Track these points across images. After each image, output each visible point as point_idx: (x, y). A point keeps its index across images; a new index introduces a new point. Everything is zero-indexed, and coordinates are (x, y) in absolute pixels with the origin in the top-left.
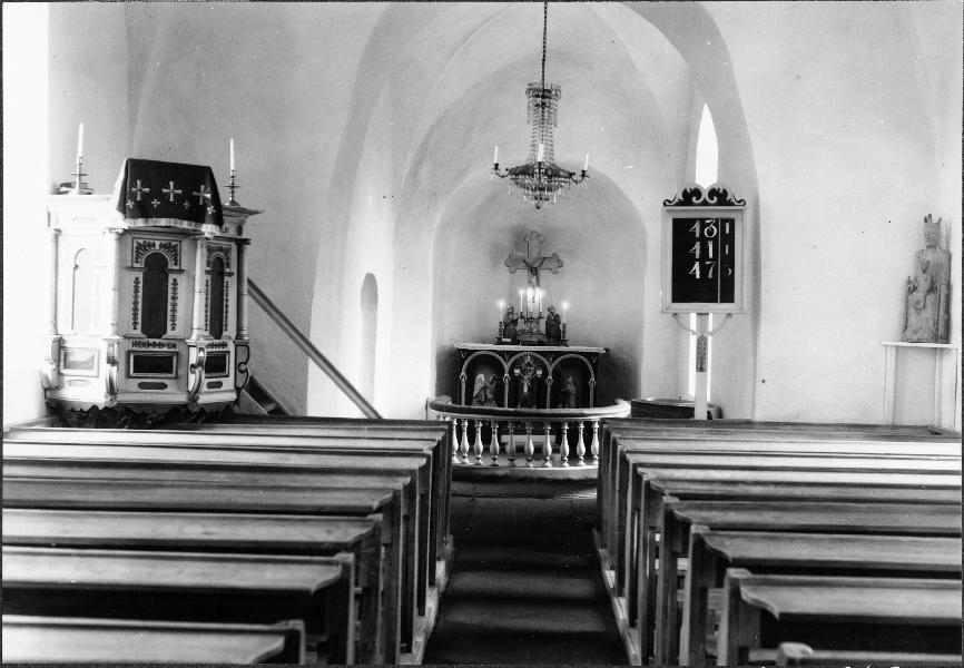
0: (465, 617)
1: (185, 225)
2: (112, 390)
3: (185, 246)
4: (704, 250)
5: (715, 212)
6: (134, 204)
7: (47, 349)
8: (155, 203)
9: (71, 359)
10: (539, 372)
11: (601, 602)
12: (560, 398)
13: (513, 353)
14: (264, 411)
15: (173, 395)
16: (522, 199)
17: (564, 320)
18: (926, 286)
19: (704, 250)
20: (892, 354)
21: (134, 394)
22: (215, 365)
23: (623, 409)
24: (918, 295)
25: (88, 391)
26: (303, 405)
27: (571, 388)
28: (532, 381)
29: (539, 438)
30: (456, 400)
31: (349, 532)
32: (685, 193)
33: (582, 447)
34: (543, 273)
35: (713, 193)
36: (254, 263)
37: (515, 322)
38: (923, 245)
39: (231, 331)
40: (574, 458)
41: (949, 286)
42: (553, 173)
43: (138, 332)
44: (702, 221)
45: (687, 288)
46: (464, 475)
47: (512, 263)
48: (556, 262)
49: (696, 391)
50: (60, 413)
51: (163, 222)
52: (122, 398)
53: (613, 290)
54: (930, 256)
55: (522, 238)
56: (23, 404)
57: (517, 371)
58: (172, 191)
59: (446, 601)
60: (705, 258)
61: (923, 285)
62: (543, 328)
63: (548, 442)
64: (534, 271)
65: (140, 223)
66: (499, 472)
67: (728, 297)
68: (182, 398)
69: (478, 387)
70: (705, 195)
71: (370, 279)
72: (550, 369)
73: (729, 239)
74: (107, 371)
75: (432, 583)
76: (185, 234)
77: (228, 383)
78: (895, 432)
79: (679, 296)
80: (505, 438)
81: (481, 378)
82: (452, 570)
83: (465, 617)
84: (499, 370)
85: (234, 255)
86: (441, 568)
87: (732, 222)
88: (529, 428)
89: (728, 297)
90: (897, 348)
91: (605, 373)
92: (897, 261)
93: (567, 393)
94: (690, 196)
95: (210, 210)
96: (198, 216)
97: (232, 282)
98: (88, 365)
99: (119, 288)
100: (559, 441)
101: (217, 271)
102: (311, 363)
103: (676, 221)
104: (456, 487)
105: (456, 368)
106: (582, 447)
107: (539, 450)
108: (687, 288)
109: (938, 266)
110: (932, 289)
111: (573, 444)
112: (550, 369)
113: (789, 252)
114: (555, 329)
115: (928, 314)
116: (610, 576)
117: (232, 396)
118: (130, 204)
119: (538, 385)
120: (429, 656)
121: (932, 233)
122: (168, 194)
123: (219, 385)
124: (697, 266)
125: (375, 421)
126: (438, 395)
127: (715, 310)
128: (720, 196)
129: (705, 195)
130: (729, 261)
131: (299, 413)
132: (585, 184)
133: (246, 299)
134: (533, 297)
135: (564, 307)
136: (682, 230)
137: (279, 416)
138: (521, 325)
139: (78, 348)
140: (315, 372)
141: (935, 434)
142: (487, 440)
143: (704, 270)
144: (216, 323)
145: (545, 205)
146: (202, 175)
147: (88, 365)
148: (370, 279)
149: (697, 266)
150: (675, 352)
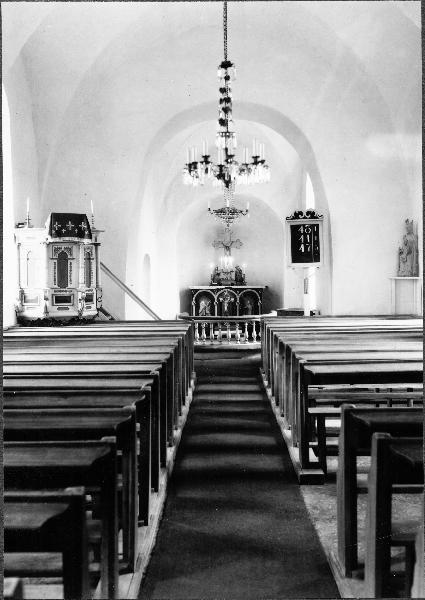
0: (193, 463)
1: (76, 239)
2: (47, 312)
3: (75, 248)
4: (305, 238)
5: (309, 222)
6: (56, 232)
7: (18, 296)
8: (64, 230)
9: (27, 299)
10: (233, 299)
11: (263, 391)
12: (244, 311)
13: (218, 290)
14: (107, 319)
15: (72, 312)
16: (220, 221)
17: (244, 272)
18: (407, 251)
19: (305, 238)
20: (394, 282)
21: (55, 313)
22: (88, 299)
23: (274, 313)
24: (404, 256)
25: (35, 312)
26: (123, 314)
27: (250, 307)
28: (229, 303)
29: (233, 332)
30: (191, 313)
31: (144, 384)
32: (295, 214)
33: (254, 334)
34: (233, 250)
35: (308, 213)
36: (103, 255)
37: (218, 274)
38: (406, 233)
39: (94, 284)
40: (251, 339)
41: (417, 252)
42: (234, 212)
43: (56, 286)
44: (304, 225)
45: (298, 257)
46: (201, 350)
47: (216, 244)
48: (239, 243)
49: (309, 305)
50: (23, 321)
51: (67, 239)
52: (51, 315)
53: (265, 260)
54: (409, 238)
55: (220, 232)
56: (9, 320)
57: (221, 299)
58: (70, 225)
59: (195, 393)
60: (306, 242)
61: (406, 252)
62: (234, 277)
63: (238, 332)
64: (227, 248)
65: (57, 240)
66: (215, 347)
67: (317, 259)
68: (76, 314)
69: (202, 307)
70: (305, 214)
71: (147, 257)
72: (238, 297)
73: (317, 234)
74: (44, 302)
75: (163, 466)
76: (76, 243)
77: (94, 306)
78: (396, 317)
79: (295, 260)
80: (217, 333)
81: (203, 304)
82: (196, 384)
83: (193, 463)
84: (213, 299)
85: (94, 251)
86: (192, 382)
87: (318, 226)
88: (228, 326)
89: (317, 259)
90: (396, 280)
91: (263, 299)
92: (396, 241)
93: (247, 309)
94: (297, 215)
95: (86, 233)
96: (81, 235)
97: (93, 262)
98: (36, 300)
99: (48, 268)
100: (244, 332)
101: (88, 259)
102: (127, 296)
103: (292, 226)
104: (195, 355)
105: (191, 298)
106: (254, 334)
107: (233, 336)
108: (298, 257)
109: (412, 243)
110: (409, 252)
111: (250, 334)
112: (238, 297)
113: (342, 240)
114: (240, 278)
115: (408, 263)
116: (266, 383)
117: (96, 312)
118: (54, 232)
119: (232, 305)
120: (146, 587)
121: (409, 227)
122: (69, 226)
123: (90, 307)
124: (302, 247)
125: (160, 322)
126: (182, 312)
127: (312, 267)
128: (311, 214)
129: (305, 214)
130: (317, 243)
131: (122, 319)
132: (248, 215)
133: (100, 271)
134: (228, 262)
135: (244, 267)
136: (295, 230)
137: (112, 321)
138: (222, 276)
139: (30, 295)
140: (128, 298)
141: (412, 317)
142: (208, 334)
143: (306, 248)
144: (88, 282)
145: (231, 225)
146: (82, 218)
147: (36, 300)
148: (147, 257)
149: (302, 247)
150: (299, 287)
